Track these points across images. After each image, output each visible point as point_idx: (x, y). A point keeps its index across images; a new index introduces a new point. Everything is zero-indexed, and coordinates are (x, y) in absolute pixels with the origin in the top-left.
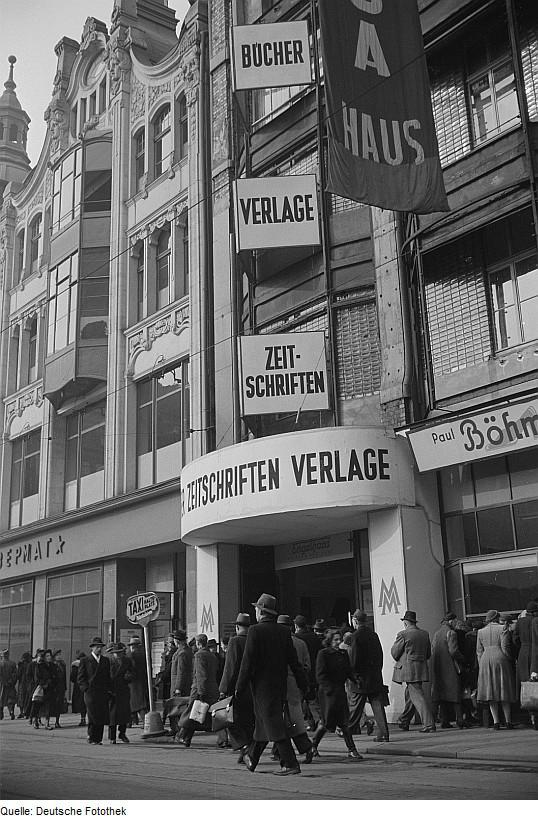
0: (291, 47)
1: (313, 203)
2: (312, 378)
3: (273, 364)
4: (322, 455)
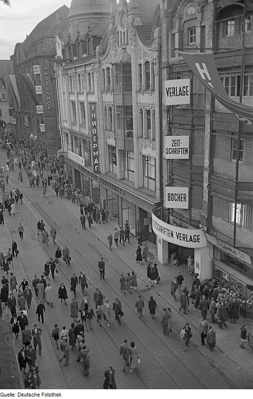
0: (183, 196)
1: (189, 89)
2: (185, 150)
3: (174, 145)
4: (183, 234)
